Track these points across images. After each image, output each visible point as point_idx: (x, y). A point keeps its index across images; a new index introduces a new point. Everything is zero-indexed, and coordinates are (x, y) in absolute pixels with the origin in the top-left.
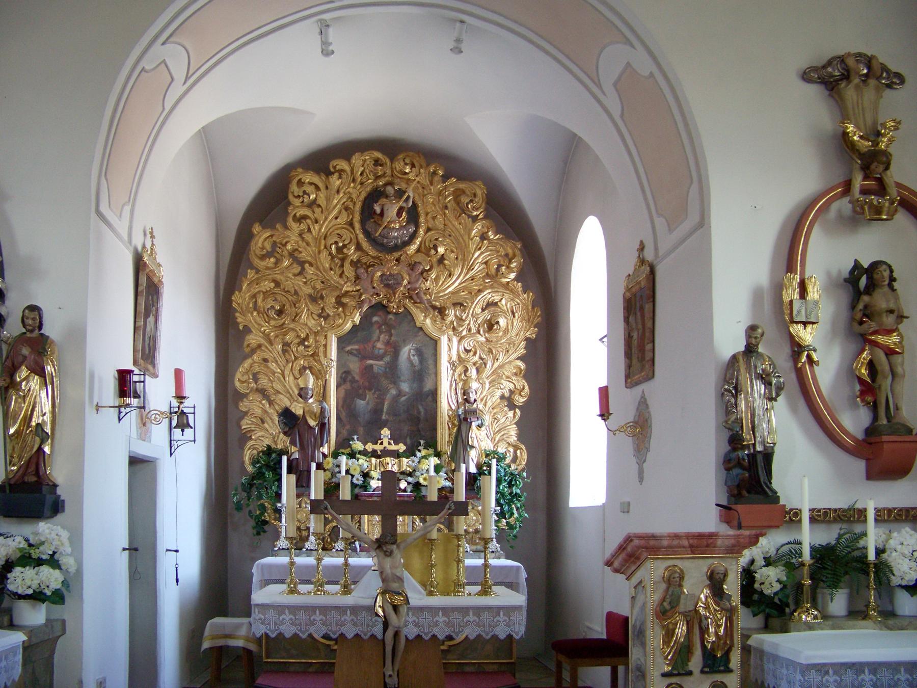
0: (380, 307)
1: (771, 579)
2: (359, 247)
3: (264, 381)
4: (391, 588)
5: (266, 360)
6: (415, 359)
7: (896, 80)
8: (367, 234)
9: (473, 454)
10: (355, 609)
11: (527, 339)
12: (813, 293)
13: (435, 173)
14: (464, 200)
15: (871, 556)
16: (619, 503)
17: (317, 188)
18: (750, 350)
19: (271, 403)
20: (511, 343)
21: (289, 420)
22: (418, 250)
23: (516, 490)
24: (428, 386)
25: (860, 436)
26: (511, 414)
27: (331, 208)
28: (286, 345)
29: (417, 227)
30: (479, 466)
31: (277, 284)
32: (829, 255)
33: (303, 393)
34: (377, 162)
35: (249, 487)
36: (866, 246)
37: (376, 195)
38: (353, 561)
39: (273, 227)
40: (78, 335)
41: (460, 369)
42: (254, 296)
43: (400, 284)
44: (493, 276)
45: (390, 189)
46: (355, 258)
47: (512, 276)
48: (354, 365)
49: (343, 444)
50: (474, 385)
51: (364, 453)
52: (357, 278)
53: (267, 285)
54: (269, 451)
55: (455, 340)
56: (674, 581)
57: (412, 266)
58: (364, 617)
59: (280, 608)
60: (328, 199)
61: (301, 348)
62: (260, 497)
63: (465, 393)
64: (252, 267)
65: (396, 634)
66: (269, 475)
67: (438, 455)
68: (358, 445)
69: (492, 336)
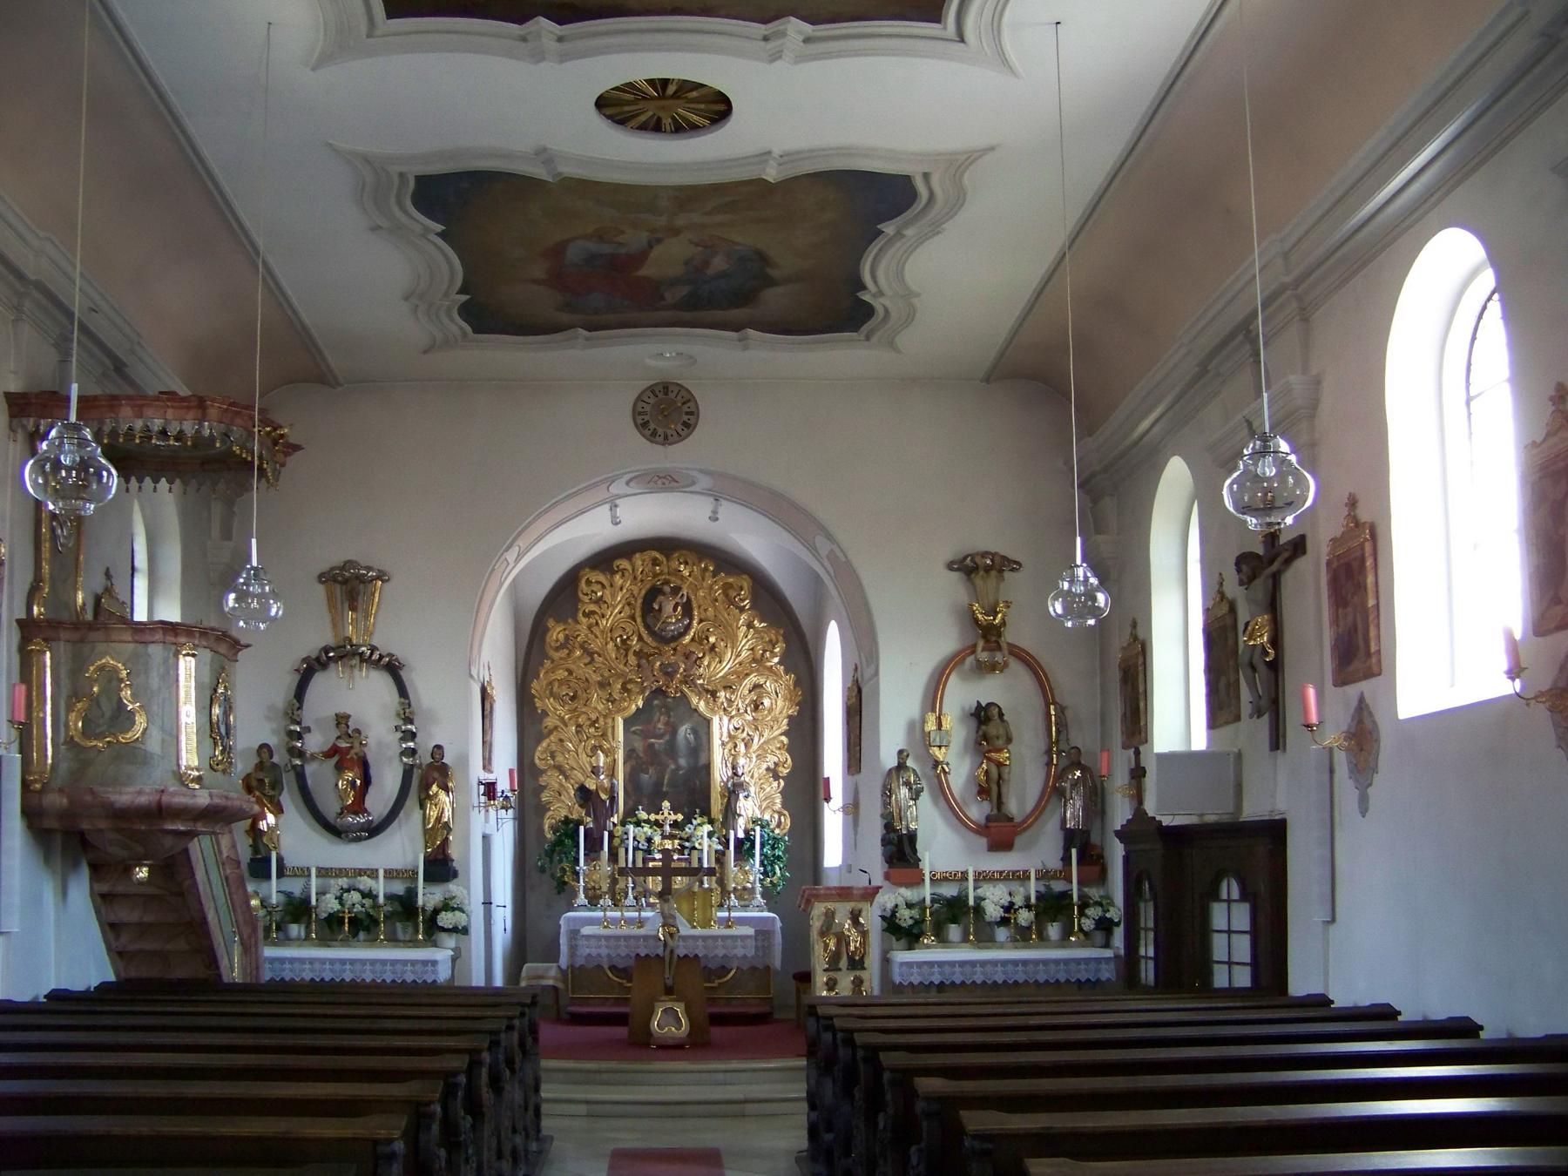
0: (659, 692)
1: (906, 917)
2: (640, 639)
3: (560, 758)
4: (668, 921)
5: (561, 740)
6: (691, 737)
7: (1012, 565)
8: (647, 627)
9: (741, 822)
10: (646, 938)
11: (790, 717)
12: (946, 725)
13: (706, 569)
14: (733, 593)
15: (971, 902)
16: (847, 867)
17: (603, 586)
18: (901, 767)
19: (567, 778)
20: (775, 720)
21: (585, 796)
22: (693, 639)
23: (777, 852)
24: (703, 761)
25: (982, 821)
26: (775, 784)
27: (614, 604)
28: (579, 726)
29: (691, 619)
30: (747, 832)
31: (570, 672)
32: (960, 695)
33: (595, 771)
34: (655, 562)
35: (550, 854)
36: (989, 690)
37: (654, 593)
38: (644, 914)
39: (566, 622)
40: (464, 760)
41: (730, 745)
42: (551, 683)
43: (676, 672)
44: (758, 661)
45: (667, 589)
46: (637, 648)
47: (776, 660)
48: (639, 745)
49: (630, 813)
50: (741, 761)
51: (647, 821)
52: (639, 666)
53: (561, 674)
54: (567, 821)
55: (726, 719)
56: (830, 915)
57: (687, 656)
58: (651, 942)
59: (598, 937)
60: (614, 596)
61: (592, 730)
62: (561, 861)
63: (734, 768)
64: (548, 658)
65: (672, 952)
66: (568, 842)
67: (711, 822)
68: (643, 815)
69: (759, 715)
